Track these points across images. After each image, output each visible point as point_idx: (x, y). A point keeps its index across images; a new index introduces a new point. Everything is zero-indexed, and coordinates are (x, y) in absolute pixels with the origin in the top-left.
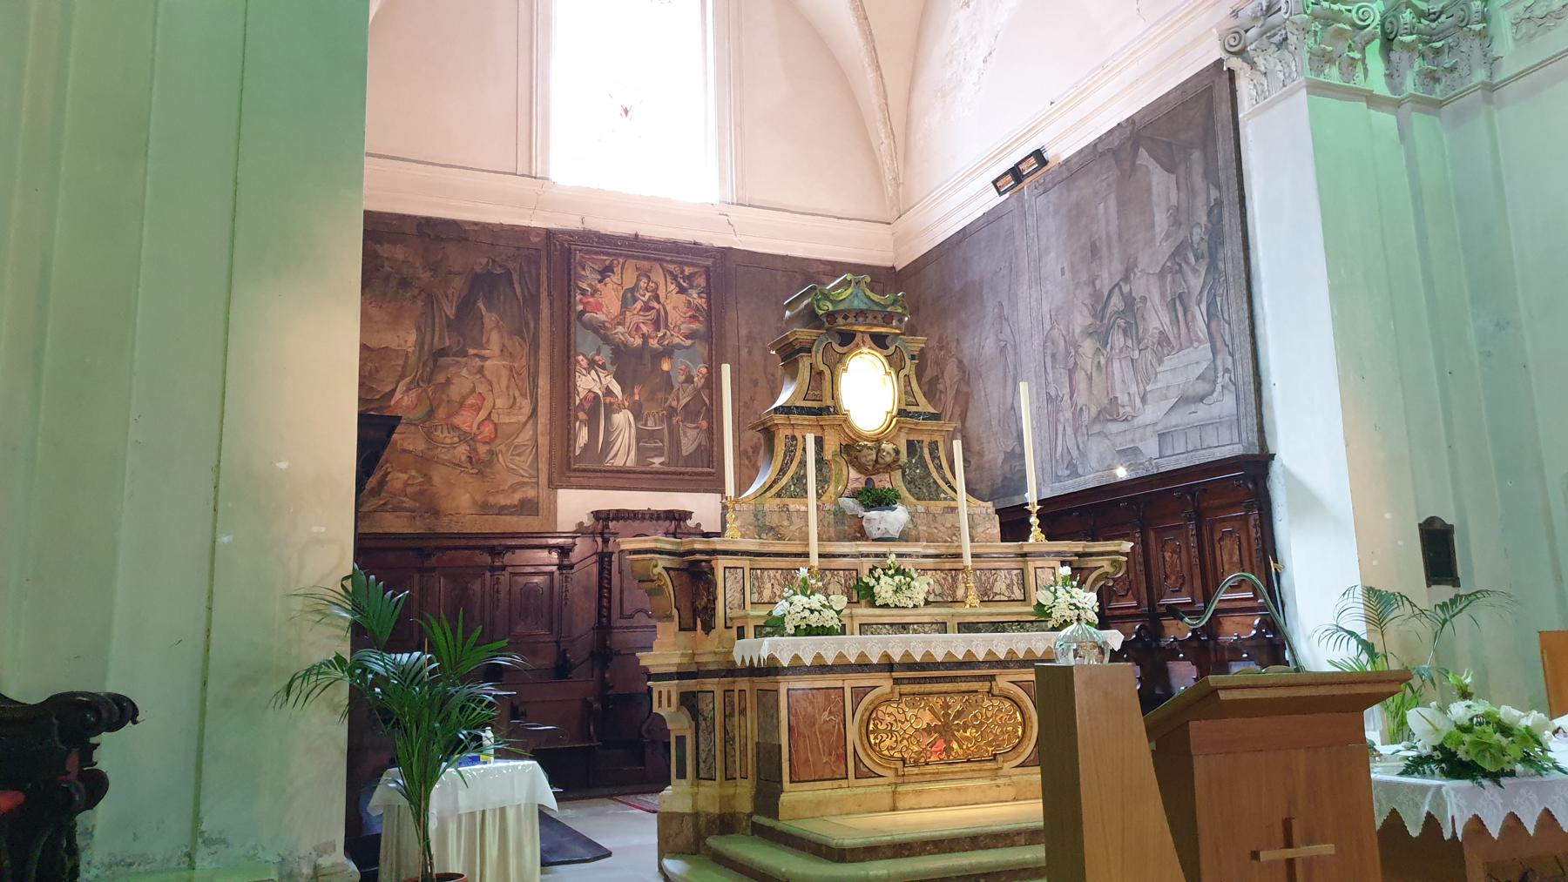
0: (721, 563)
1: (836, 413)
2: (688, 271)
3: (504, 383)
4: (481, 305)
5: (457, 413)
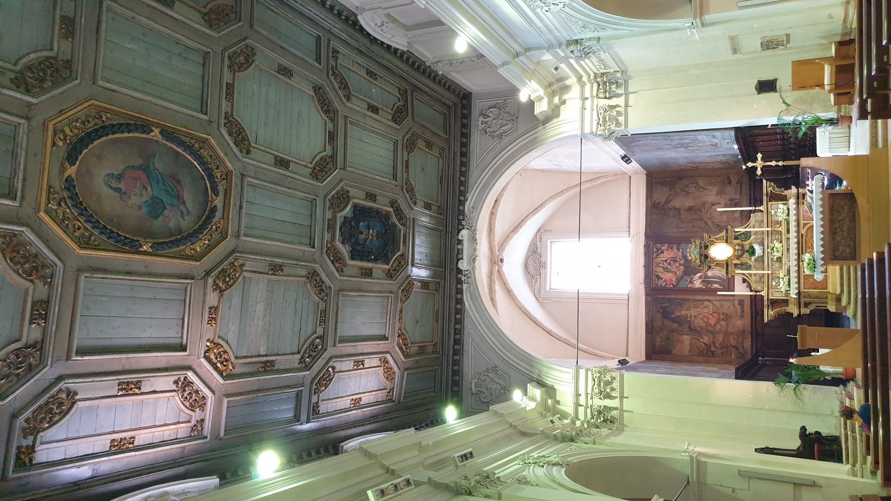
0: (771, 297)
1: (728, 260)
2: (655, 250)
3: (699, 310)
4: (673, 316)
5: (710, 324)
